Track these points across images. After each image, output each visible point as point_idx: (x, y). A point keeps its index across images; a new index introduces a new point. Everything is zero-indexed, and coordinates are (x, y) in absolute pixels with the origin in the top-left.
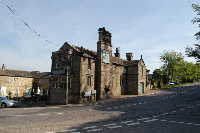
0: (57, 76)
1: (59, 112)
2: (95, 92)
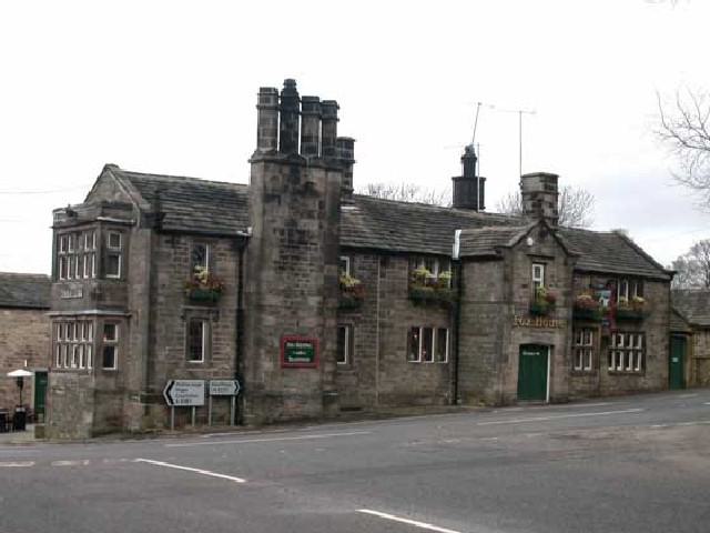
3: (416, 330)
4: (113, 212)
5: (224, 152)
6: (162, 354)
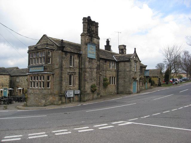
0: (34, 74)
1: (16, 116)
2: (78, 92)
3: (110, 77)
4: (49, 46)
5: (73, 34)
6: (64, 83)
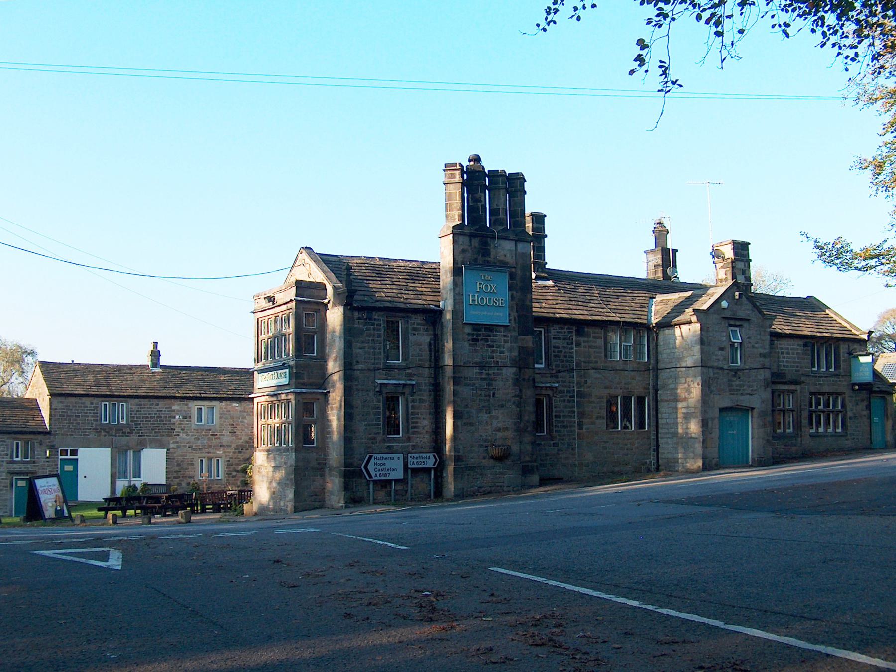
5: (420, 233)
